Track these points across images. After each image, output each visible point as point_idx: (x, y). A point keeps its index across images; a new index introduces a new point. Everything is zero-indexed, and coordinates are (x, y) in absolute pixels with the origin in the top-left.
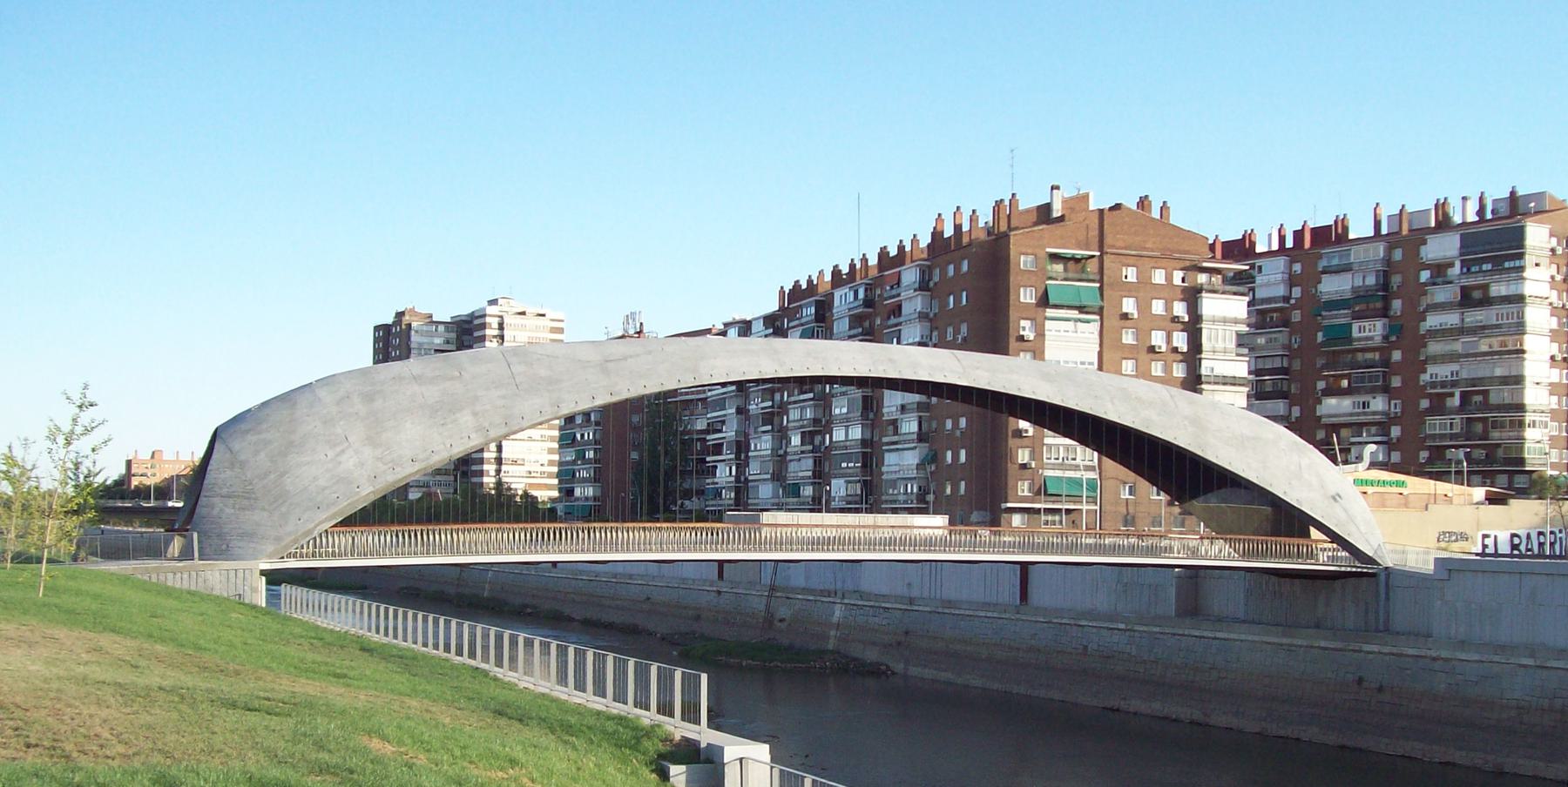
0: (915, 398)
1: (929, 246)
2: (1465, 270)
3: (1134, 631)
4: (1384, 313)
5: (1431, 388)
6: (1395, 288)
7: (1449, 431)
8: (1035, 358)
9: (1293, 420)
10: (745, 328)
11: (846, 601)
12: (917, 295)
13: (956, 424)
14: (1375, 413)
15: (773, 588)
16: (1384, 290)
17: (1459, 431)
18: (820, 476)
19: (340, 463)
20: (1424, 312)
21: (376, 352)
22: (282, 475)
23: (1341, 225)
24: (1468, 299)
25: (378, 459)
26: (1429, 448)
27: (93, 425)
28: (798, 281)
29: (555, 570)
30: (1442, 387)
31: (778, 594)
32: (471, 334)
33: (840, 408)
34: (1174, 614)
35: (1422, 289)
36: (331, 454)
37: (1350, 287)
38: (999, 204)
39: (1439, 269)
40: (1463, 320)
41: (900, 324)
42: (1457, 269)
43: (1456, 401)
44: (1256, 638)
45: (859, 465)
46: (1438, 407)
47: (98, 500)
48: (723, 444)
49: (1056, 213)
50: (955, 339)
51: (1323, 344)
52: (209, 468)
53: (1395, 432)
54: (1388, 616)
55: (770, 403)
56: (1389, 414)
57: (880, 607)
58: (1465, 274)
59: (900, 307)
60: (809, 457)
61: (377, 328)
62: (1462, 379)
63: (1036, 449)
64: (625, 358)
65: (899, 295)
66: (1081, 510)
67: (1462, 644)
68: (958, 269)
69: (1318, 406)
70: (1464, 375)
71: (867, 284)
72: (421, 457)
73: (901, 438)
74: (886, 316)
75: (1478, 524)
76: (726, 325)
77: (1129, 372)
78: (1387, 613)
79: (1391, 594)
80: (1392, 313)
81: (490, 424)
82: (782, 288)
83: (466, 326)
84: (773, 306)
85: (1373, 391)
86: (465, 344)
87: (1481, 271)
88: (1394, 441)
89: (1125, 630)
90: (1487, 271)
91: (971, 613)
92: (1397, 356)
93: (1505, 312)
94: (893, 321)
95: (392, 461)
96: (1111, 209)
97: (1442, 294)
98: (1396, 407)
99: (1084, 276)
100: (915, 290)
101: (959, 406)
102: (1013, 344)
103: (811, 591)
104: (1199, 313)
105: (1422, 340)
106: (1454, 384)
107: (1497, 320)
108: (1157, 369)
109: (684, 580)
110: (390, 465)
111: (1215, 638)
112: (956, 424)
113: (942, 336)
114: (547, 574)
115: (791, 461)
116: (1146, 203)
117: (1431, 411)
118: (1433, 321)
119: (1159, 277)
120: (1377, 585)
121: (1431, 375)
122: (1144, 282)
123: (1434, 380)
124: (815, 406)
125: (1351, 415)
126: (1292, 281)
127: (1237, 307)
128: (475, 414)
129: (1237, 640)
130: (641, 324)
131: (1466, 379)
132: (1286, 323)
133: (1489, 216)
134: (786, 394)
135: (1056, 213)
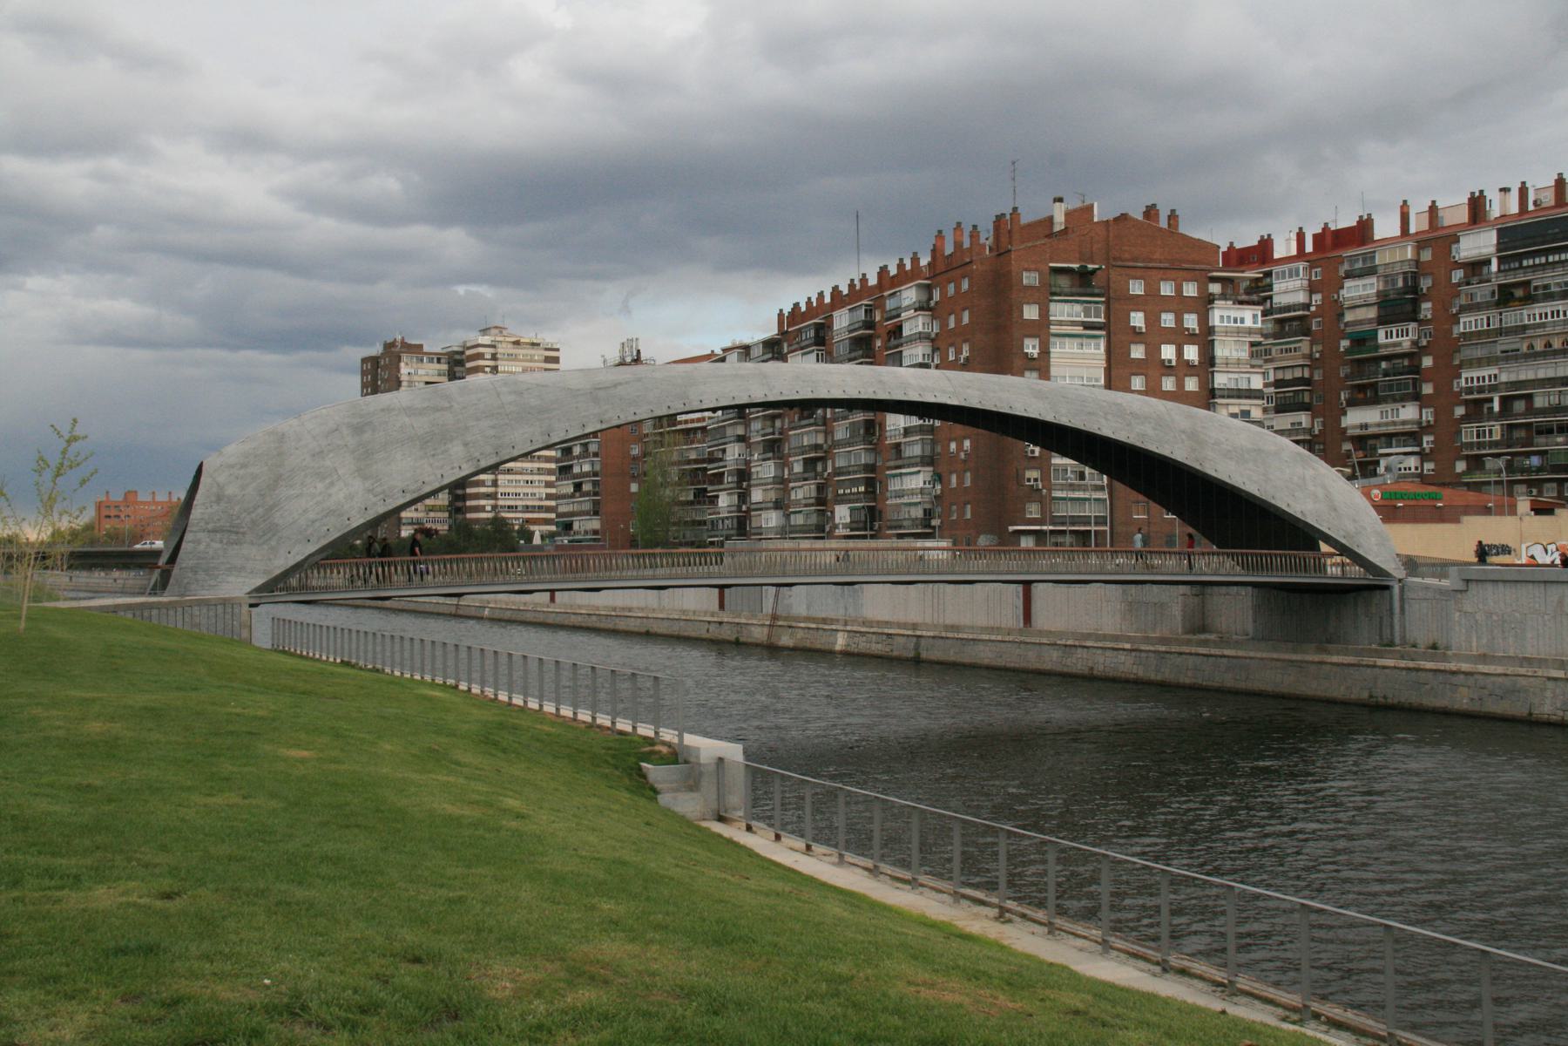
0: (915, 421)
1: (929, 264)
3: (1141, 651)
5: (1466, 394)
6: (1425, 291)
7: (1475, 440)
8: (1040, 378)
9: (1317, 432)
10: (745, 351)
11: (849, 628)
13: (960, 447)
14: (1404, 423)
15: (775, 617)
16: (1412, 293)
17: (1499, 438)
18: (822, 502)
19: (330, 495)
20: (1457, 314)
21: (364, 385)
22: (271, 508)
23: (1362, 231)
24: (1506, 297)
25: (369, 491)
26: (1467, 458)
27: (79, 459)
28: (798, 303)
29: (552, 605)
30: (1479, 392)
31: (780, 623)
32: (463, 365)
33: (841, 432)
34: (1180, 630)
35: (1454, 291)
36: (320, 486)
37: (1375, 291)
38: (999, 219)
39: (1476, 267)
41: (901, 345)
42: (1494, 267)
43: (1496, 407)
44: (1264, 655)
46: (1477, 409)
48: (723, 473)
49: (1057, 228)
50: (957, 359)
51: (1348, 351)
52: (195, 502)
53: (1427, 440)
54: (1405, 628)
55: (771, 430)
56: (1421, 423)
57: (882, 634)
59: (899, 328)
61: (364, 360)
63: (1044, 467)
64: (615, 386)
65: (899, 316)
66: (1090, 531)
67: (1484, 658)
68: (958, 288)
69: (1343, 418)
70: (1504, 378)
71: (866, 305)
72: (412, 487)
73: (906, 462)
74: (886, 338)
76: (725, 350)
77: (1138, 388)
78: (1403, 627)
79: (1407, 606)
80: (1422, 317)
81: (481, 454)
82: (781, 310)
83: (458, 357)
84: (772, 331)
85: (1403, 399)
86: (457, 375)
87: (1521, 267)
89: (1131, 650)
90: (1528, 267)
91: (975, 636)
92: (1427, 362)
93: (1537, 312)
94: (893, 342)
95: (384, 492)
96: (1116, 219)
97: (1482, 292)
98: (1428, 415)
100: (916, 310)
101: (959, 429)
102: (1018, 362)
103: (813, 620)
104: (1210, 324)
105: (1455, 345)
106: (1493, 388)
107: (1529, 320)
108: (1168, 384)
109: (684, 612)
110: (382, 496)
111: (1223, 656)
112: (960, 447)
113: (944, 357)
114: (545, 609)
116: (1152, 212)
117: (1466, 418)
119: (1167, 289)
120: (1391, 598)
121: (1467, 379)
122: (1152, 294)
123: (1470, 385)
125: (1379, 425)
126: (1312, 289)
127: (1250, 317)
128: (466, 445)
129: (1246, 658)
130: (639, 351)
131: (1507, 383)
132: (1307, 332)
133: (1531, 207)
134: (787, 420)
135: (1057, 228)
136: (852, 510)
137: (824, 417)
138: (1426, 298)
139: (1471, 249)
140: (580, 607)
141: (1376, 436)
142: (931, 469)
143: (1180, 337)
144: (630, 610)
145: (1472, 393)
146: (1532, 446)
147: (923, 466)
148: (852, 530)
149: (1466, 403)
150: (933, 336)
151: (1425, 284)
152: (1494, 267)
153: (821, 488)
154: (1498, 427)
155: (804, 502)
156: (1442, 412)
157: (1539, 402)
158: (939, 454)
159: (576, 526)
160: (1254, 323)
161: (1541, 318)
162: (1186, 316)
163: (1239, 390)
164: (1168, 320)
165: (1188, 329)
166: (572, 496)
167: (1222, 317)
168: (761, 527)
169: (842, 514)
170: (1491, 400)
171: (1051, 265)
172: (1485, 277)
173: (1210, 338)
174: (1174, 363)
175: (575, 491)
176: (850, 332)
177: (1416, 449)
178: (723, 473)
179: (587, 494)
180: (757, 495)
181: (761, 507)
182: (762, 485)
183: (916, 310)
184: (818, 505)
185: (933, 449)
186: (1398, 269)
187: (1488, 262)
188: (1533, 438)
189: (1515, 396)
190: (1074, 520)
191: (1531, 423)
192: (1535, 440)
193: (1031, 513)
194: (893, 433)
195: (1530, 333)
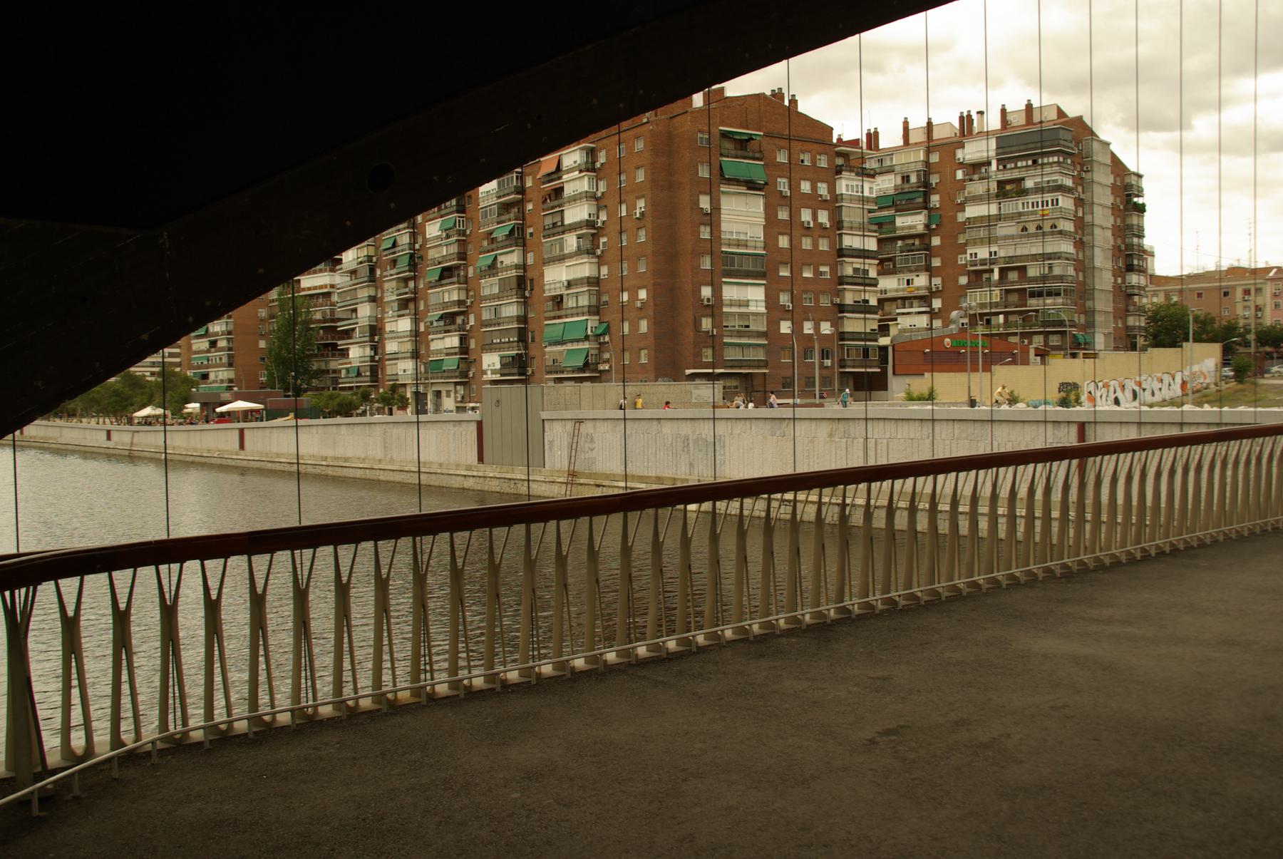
2: (1001, 167)
4: (926, 206)
6: (934, 186)
12: (583, 176)
14: (918, 288)
24: (1006, 190)
35: (961, 185)
39: (976, 168)
40: (1000, 208)
42: (994, 166)
43: (996, 276)
45: (516, 339)
46: (978, 277)
47: (323, 367)
53: (937, 304)
58: (1001, 170)
60: (455, 336)
62: (1000, 258)
70: (1002, 253)
75: (1084, 376)
85: (917, 270)
87: (1016, 167)
88: (937, 311)
92: (936, 241)
93: (1030, 201)
97: (978, 188)
99: (746, 154)
100: (581, 171)
106: (993, 262)
107: (1023, 208)
115: (432, 340)
117: (969, 285)
118: (972, 211)
121: (971, 254)
124: (459, 289)
125: (897, 290)
136: (502, 357)
137: (466, 276)
138: (935, 191)
139: (973, 153)
140: (278, 455)
141: (894, 299)
142: (597, 318)
143: (815, 202)
144: (346, 460)
145: (976, 265)
146: (1026, 306)
147: (589, 315)
148: (502, 375)
149: (969, 273)
150: (599, 194)
151: (934, 179)
152: (994, 166)
153: (464, 340)
154: (998, 292)
155: (445, 351)
156: (949, 281)
157: (1032, 272)
158: (606, 303)
159: (212, 376)
160: (870, 193)
161: (1033, 207)
162: (819, 185)
163: (864, 250)
164: (805, 187)
165: (821, 196)
166: (208, 351)
167: (847, 186)
168: (397, 374)
169: (491, 361)
170: (992, 271)
171: (721, 128)
172: (985, 175)
173: (837, 205)
174: (812, 225)
175: (210, 347)
176: (499, 197)
177: (928, 309)
178: (353, 329)
179: (222, 349)
180: (391, 347)
181: (396, 357)
182: (398, 338)
183: (581, 171)
184: (461, 354)
185: (599, 299)
186: (912, 167)
187: (989, 163)
188: (1026, 300)
189: (1014, 267)
190: (740, 363)
191: (1025, 289)
192: (1028, 302)
193: (707, 357)
194: (553, 286)
195: (1023, 218)
